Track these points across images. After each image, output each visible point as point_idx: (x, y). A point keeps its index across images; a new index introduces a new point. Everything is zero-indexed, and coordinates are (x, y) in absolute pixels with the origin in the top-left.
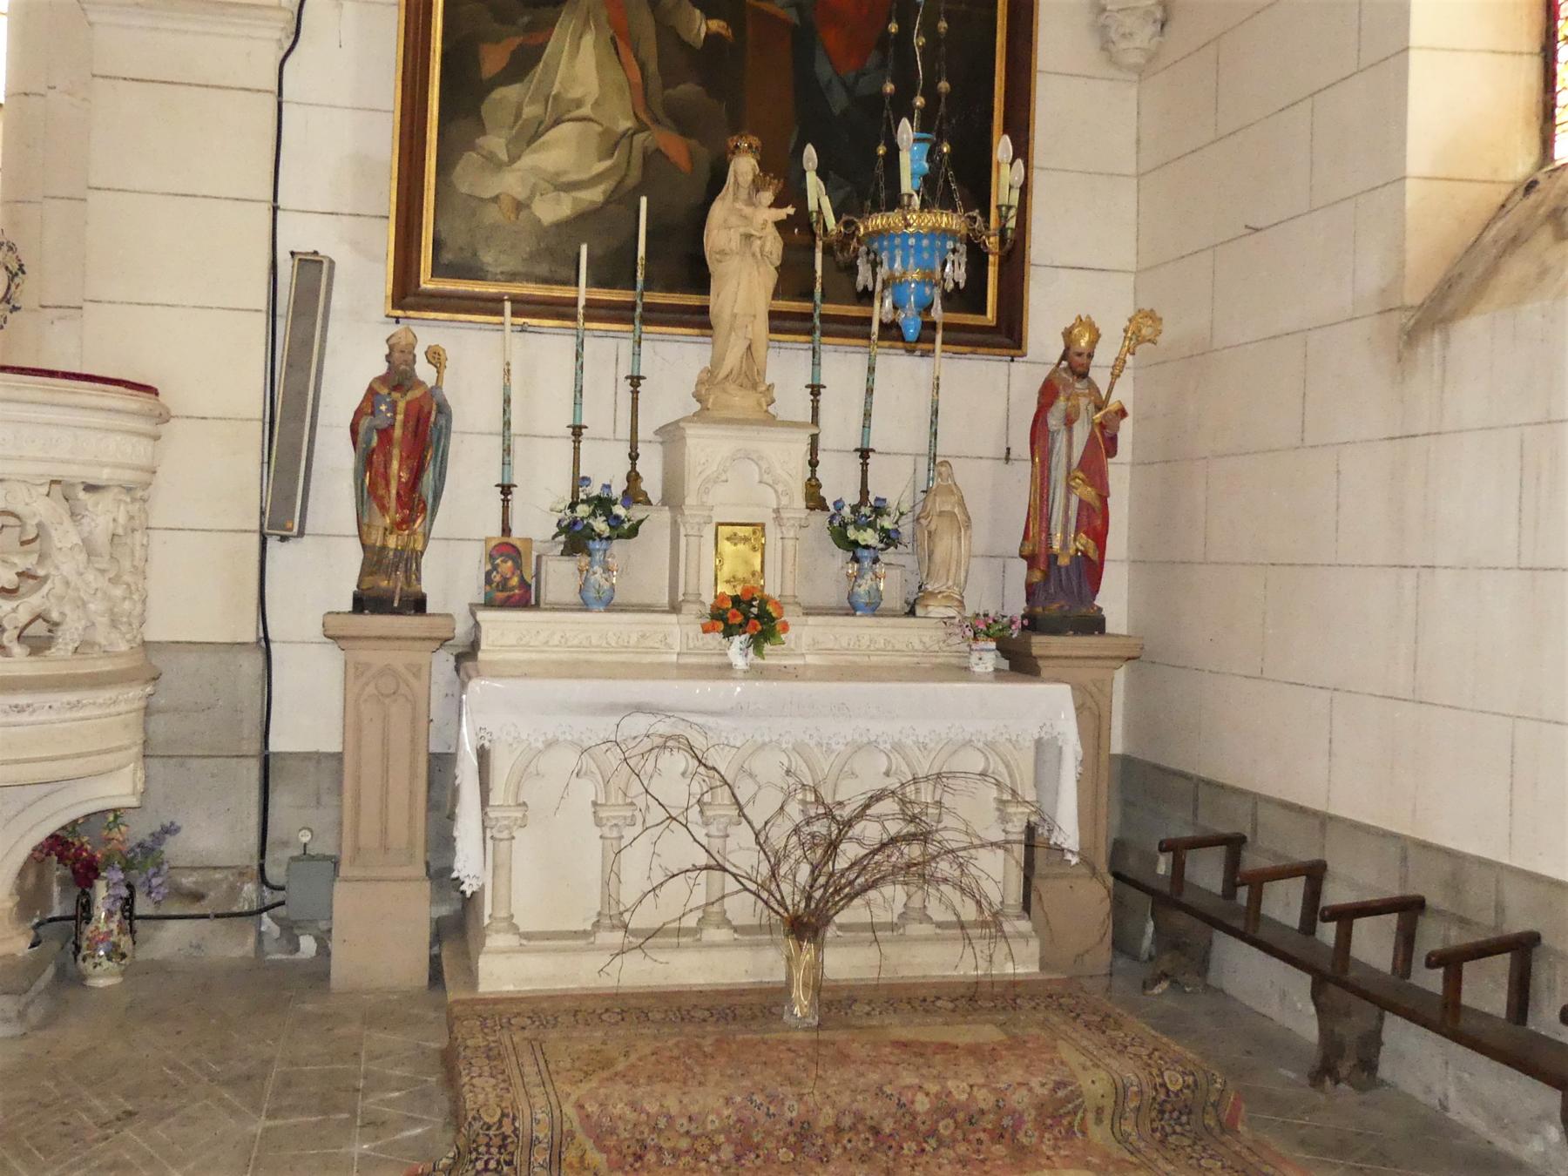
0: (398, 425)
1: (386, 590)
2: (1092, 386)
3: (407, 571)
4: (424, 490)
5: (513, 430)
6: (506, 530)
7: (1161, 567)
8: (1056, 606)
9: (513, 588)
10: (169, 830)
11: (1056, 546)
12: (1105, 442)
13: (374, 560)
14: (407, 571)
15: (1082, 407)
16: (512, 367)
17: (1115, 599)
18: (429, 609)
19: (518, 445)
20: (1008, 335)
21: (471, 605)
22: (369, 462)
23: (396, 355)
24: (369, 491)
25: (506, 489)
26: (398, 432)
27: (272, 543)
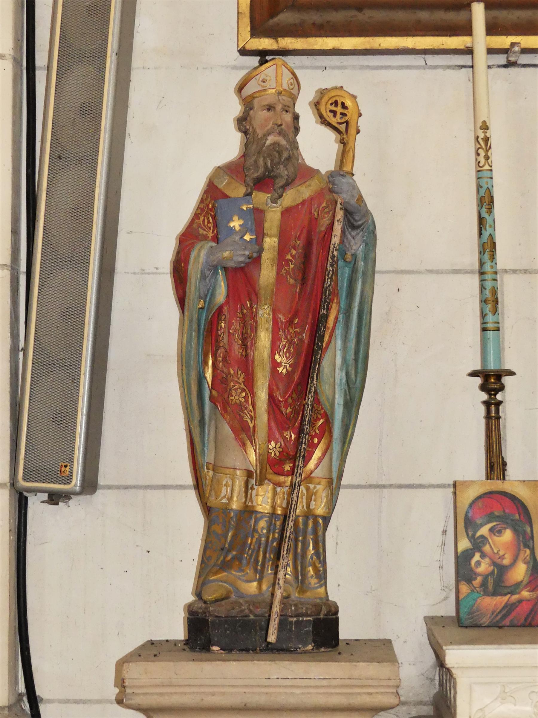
0: (268, 256)
1: (253, 602)
3: (299, 561)
4: (325, 389)
5: (503, 259)
6: (496, 465)
9: (516, 588)
13: (228, 540)
14: (299, 561)
16: (494, 134)
18: (345, 632)
19: (510, 290)
21: (431, 622)
22: (212, 337)
23: (260, 116)
24: (213, 394)
25: (492, 381)
26: (267, 274)
27: (36, 506)
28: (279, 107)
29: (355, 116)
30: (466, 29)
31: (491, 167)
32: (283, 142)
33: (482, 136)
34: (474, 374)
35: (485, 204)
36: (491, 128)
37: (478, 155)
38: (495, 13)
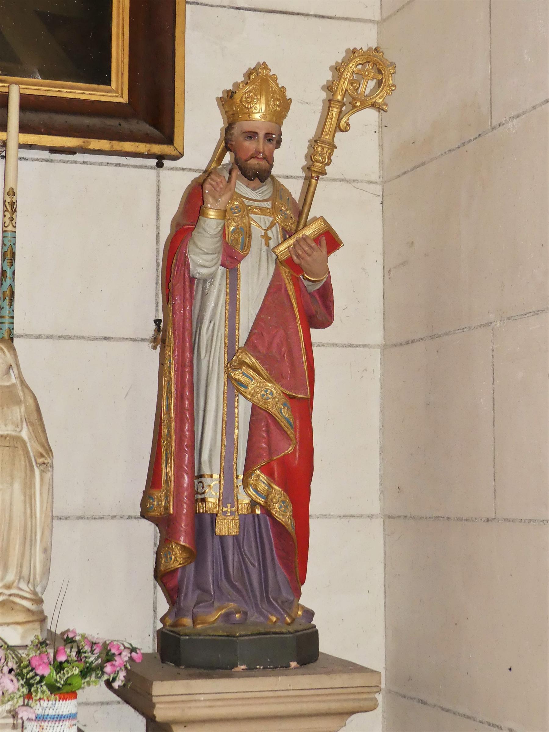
2: (279, 192)
7: (428, 524)
8: (215, 616)
11: (212, 498)
12: (304, 301)
15: (257, 232)
17: (346, 593)
20: (152, 116)
31: (15, 227)
33: (8, 200)
35: (7, 258)
36: (19, 193)
37: (5, 216)
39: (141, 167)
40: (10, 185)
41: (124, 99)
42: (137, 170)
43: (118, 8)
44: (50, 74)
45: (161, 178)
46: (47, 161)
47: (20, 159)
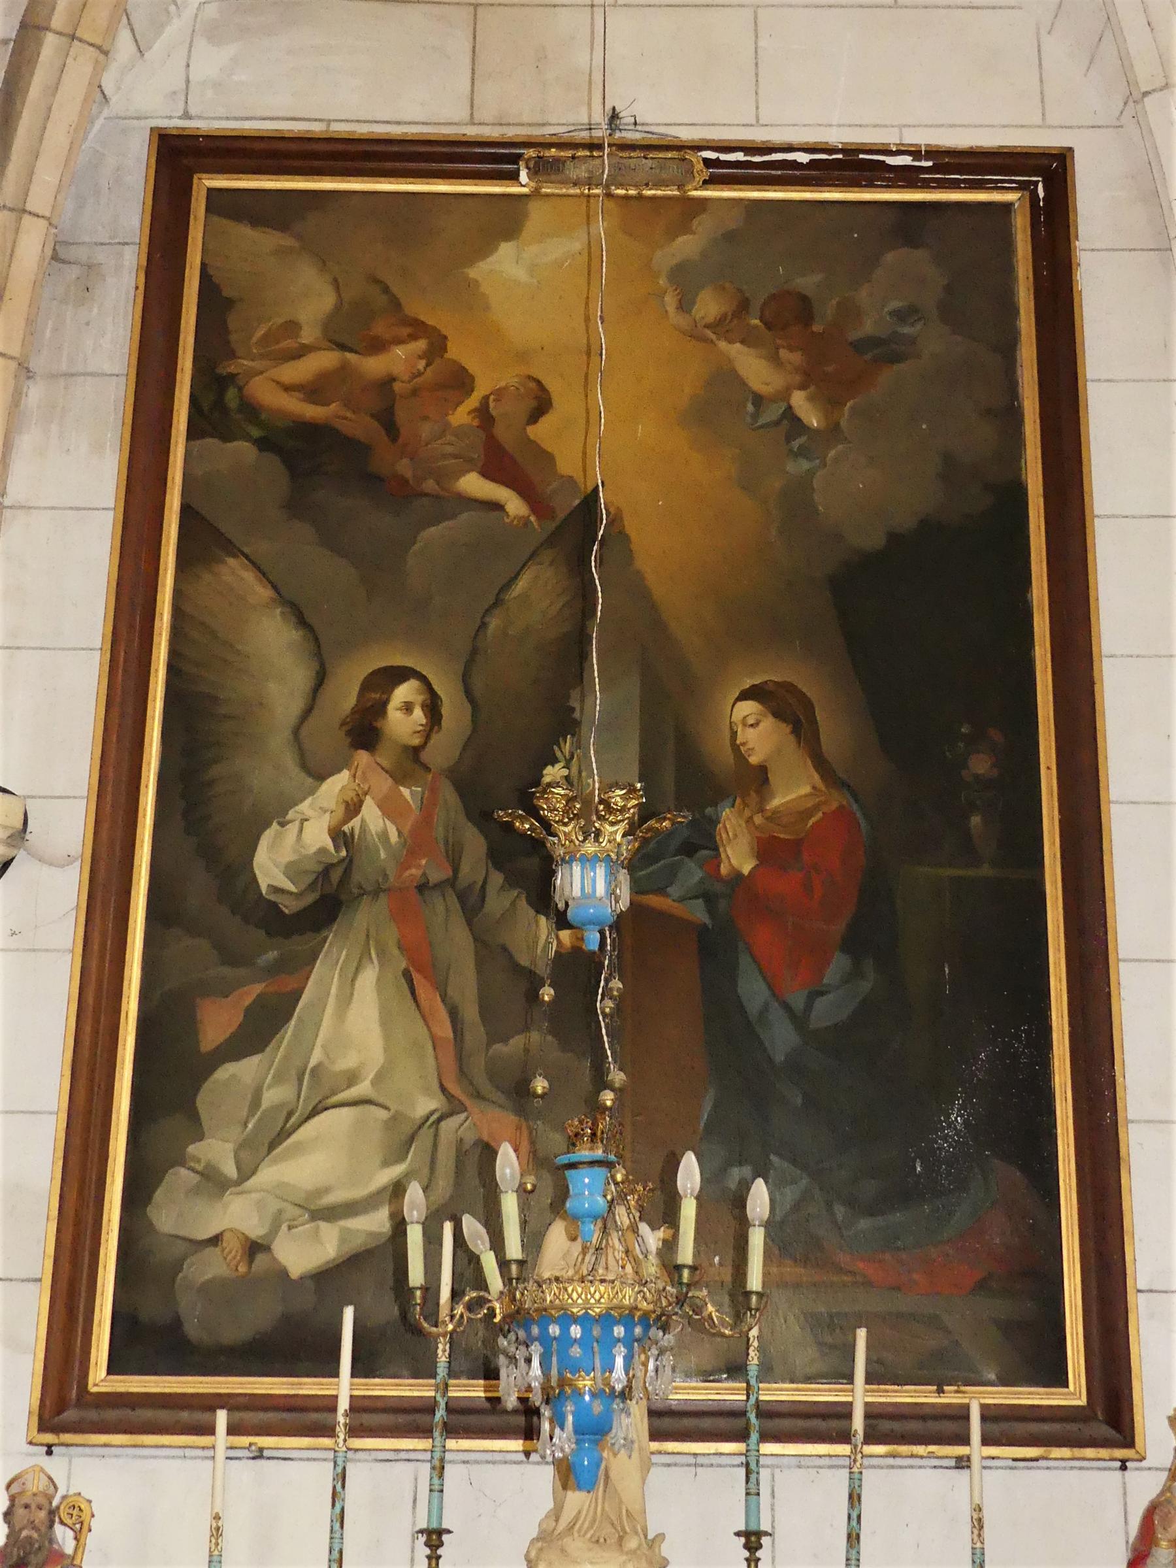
10: (449, 1532)
23: (20, 1512)
28: (33, 1507)
29: (89, 1515)
30: (210, 1430)
32: (35, 1535)
33: (975, 1516)
34: (738, 1534)
38: (238, 1415)
39: (1105, 1469)
40: (977, 1501)
41: (1082, 1401)
42: (1102, 1472)
43: (1072, 1335)
44: (1005, 1380)
45: (1127, 1480)
46: (1011, 1468)
47: (984, 1468)
